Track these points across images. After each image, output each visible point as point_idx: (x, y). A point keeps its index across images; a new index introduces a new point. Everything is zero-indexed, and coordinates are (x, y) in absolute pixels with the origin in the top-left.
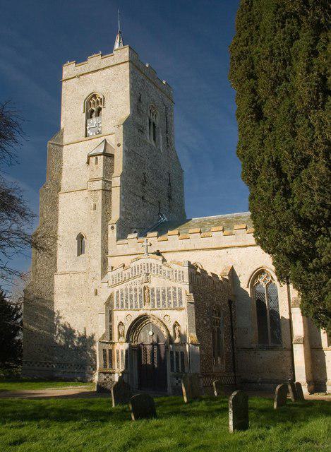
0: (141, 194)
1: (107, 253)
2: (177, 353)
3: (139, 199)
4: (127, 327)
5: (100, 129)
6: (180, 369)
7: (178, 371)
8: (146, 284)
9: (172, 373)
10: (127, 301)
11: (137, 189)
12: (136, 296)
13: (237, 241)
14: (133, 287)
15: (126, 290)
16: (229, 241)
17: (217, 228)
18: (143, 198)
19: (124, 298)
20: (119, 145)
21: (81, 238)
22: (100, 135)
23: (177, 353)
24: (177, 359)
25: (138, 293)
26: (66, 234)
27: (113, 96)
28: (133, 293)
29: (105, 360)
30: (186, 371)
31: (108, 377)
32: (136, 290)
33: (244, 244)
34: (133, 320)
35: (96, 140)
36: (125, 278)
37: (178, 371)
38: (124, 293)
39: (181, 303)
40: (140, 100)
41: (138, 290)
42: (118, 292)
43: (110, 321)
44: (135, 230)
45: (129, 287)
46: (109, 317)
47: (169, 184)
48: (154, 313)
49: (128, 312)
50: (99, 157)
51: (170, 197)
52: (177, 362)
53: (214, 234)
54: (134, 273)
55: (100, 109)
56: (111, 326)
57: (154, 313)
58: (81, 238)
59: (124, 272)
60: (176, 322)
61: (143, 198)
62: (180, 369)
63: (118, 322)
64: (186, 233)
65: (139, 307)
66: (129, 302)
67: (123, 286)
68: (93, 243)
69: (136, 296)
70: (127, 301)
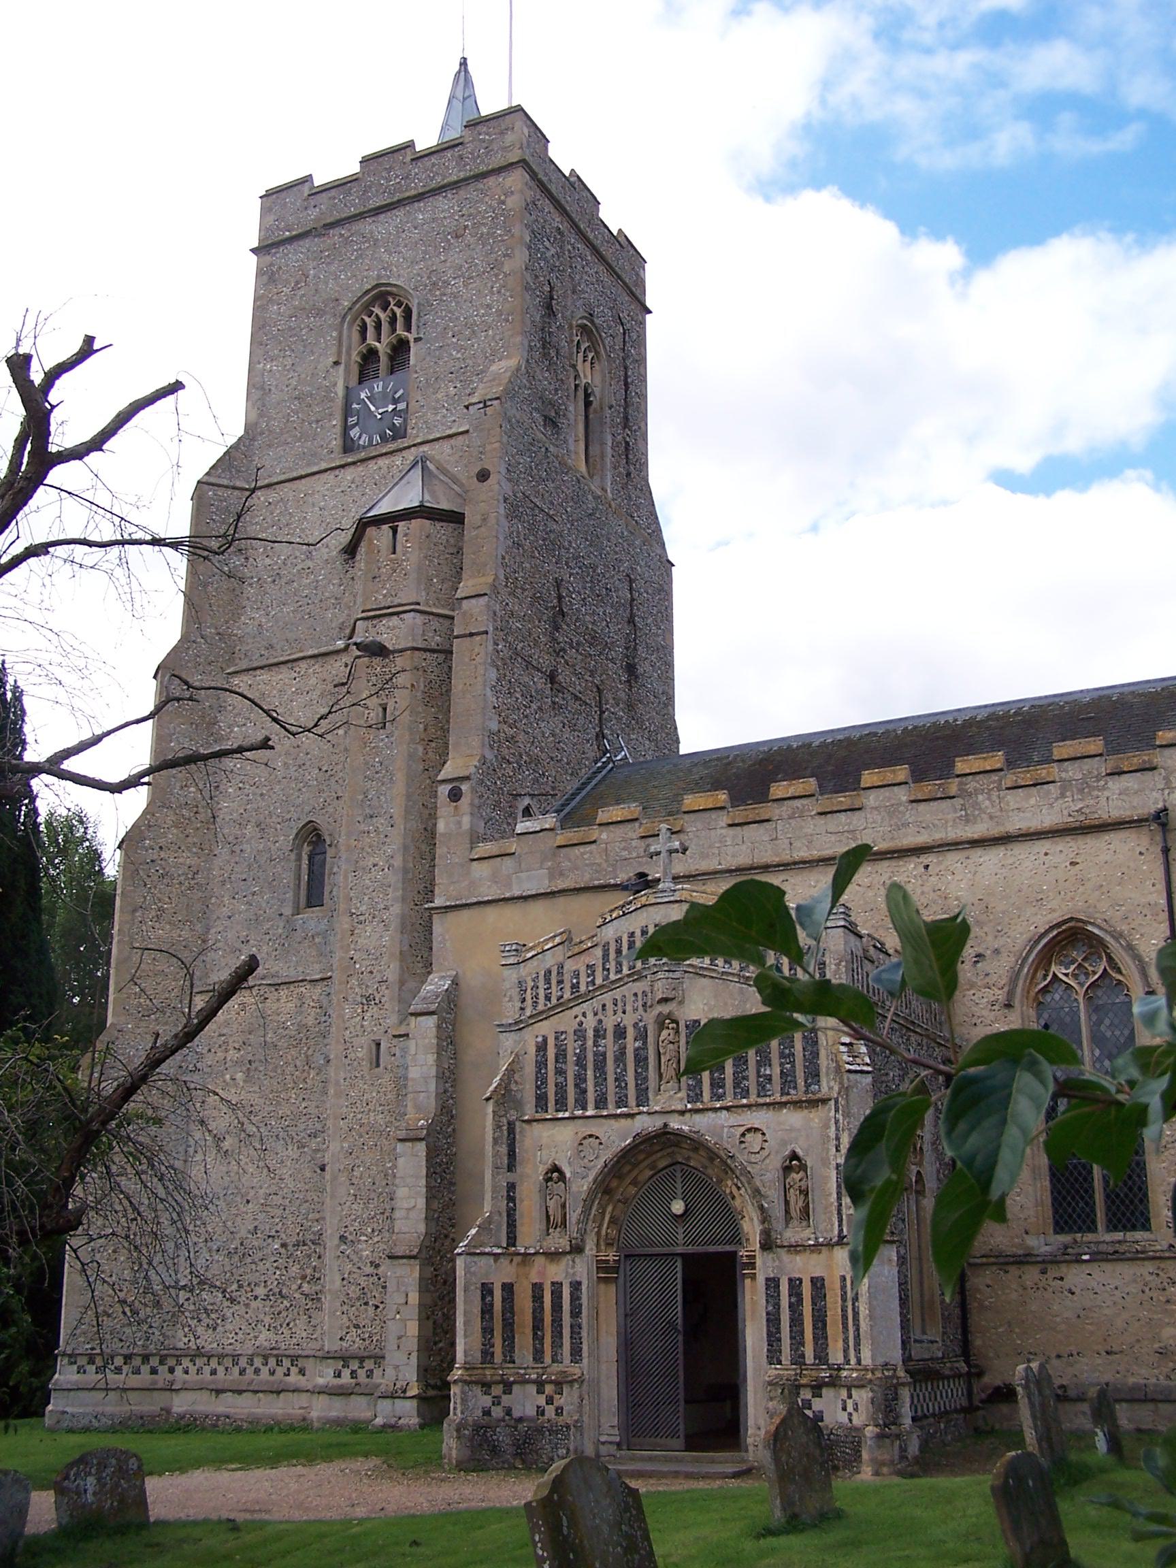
0: (546, 661)
1: (429, 893)
2: (795, 1284)
3: (540, 682)
4: (582, 1186)
5: (397, 421)
6: (809, 1351)
7: (798, 1359)
8: (665, 1009)
9: (773, 1371)
10: (580, 1079)
11: (536, 642)
12: (620, 1056)
13: (967, 820)
14: (609, 1023)
15: (580, 1034)
16: (938, 821)
17: (797, 787)
18: (552, 678)
19: (571, 1070)
20: (483, 476)
21: (313, 840)
22: (401, 443)
23: (795, 1285)
24: (795, 1307)
25: (631, 1044)
26: (250, 830)
27: (455, 296)
28: (609, 1045)
29: (487, 1331)
30: (836, 1357)
31: (497, 1401)
32: (620, 1033)
33: (996, 831)
34: (607, 1155)
35: (382, 462)
36: (575, 987)
37: (798, 1359)
38: (572, 1047)
39: (813, 1075)
40: (549, 307)
41: (631, 1033)
42: (542, 1047)
43: (511, 1167)
44: (527, 801)
45: (590, 1023)
46: (504, 1149)
47: (631, 621)
48: (702, 1123)
49: (586, 1128)
50: (402, 526)
51: (631, 669)
52: (796, 1321)
53: (871, 799)
54: (612, 965)
55: (400, 349)
56: (511, 1187)
57: (702, 1123)
58: (313, 840)
59: (570, 966)
60: (794, 1156)
61: (552, 678)
62: (809, 1351)
63: (542, 1169)
64: (1049, 760)
65: (632, 1101)
66: (590, 1085)
67: (566, 1022)
68: (369, 877)
69: (620, 1056)
70: (580, 1079)
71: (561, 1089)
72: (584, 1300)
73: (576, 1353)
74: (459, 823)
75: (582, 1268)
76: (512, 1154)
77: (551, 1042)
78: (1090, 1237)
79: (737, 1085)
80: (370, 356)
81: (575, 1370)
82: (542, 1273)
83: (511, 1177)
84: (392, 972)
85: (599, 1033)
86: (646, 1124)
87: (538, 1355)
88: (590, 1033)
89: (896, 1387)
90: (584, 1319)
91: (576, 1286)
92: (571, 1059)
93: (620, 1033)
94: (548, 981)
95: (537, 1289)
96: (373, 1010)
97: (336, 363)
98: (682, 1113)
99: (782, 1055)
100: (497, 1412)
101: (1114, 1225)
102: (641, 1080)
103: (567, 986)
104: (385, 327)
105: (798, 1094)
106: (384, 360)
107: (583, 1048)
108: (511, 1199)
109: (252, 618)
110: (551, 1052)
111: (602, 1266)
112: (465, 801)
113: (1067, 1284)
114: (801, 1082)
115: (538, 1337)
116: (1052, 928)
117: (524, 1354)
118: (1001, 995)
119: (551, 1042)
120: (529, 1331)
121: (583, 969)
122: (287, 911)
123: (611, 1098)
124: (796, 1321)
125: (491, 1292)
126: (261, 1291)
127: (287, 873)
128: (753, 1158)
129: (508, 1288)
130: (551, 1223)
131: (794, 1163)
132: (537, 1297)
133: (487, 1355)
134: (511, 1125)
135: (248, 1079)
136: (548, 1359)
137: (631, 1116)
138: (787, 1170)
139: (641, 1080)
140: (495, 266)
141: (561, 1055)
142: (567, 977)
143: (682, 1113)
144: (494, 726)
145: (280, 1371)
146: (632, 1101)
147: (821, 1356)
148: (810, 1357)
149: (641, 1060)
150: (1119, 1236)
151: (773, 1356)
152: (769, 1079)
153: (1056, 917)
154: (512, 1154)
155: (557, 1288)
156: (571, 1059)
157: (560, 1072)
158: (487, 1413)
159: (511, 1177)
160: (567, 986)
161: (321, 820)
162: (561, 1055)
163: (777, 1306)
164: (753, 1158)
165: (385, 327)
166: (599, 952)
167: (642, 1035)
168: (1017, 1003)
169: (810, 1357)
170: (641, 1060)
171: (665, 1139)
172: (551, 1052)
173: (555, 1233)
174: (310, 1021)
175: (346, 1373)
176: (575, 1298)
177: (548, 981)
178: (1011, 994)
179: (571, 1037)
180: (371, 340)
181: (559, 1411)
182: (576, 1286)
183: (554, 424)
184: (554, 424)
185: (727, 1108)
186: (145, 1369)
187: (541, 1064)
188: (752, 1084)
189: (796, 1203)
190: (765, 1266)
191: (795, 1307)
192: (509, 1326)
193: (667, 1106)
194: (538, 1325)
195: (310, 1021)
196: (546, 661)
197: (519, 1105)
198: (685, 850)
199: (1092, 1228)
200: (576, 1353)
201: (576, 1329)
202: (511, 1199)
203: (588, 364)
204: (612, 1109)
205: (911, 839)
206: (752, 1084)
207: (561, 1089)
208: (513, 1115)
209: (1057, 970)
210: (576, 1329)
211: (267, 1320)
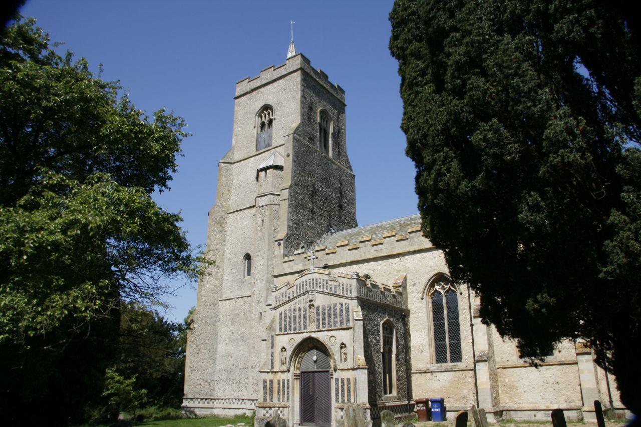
0: (310, 206)
6: (346, 398)
7: (343, 401)
10: (290, 323)
12: (300, 317)
18: (312, 211)
19: (288, 320)
24: (284, 386)
27: (284, 106)
30: (352, 401)
31: (267, 412)
32: (300, 310)
33: (420, 248)
34: (296, 344)
36: (289, 297)
37: (343, 401)
38: (288, 315)
39: (348, 320)
41: (302, 310)
42: (281, 314)
43: (272, 348)
44: (302, 245)
45: (293, 307)
51: (340, 206)
52: (343, 390)
55: (271, 121)
56: (272, 353)
58: (248, 257)
61: (312, 211)
62: (346, 398)
63: (281, 348)
65: (302, 328)
66: (292, 324)
67: (286, 307)
71: (285, 325)
72: (290, 385)
73: (288, 399)
74: (280, 252)
75: (289, 376)
76: (273, 344)
77: (283, 313)
78: (445, 364)
79: (329, 324)
80: (263, 125)
81: (288, 404)
82: (280, 377)
83: (272, 350)
84: (264, 293)
85: (295, 310)
86: (305, 335)
87: (279, 399)
88: (293, 310)
89: (366, 409)
90: (290, 390)
91: (288, 381)
92: (288, 317)
93: (300, 310)
94: (283, 295)
95: (279, 381)
96: (260, 304)
97: (255, 127)
98: (315, 332)
99: (340, 315)
100: (267, 415)
101: (452, 361)
102: (305, 322)
103: (287, 297)
104: (267, 116)
105: (344, 326)
106: (267, 125)
107: (291, 315)
108: (272, 356)
109: (233, 198)
110: (283, 315)
111: (295, 375)
112: (282, 246)
113: (438, 378)
114: (345, 323)
115: (279, 395)
116: (434, 276)
117: (275, 400)
118: (420, 295)
119: (283, 313)
120: (277, 393)
121: (291, 292)
122: (242, 277)
123: (298, 328)
124: (343, 390)
125: (266, 382)
126: (235, 381)
127: (242, 265)
128: (333, 344)
129: (271, 381)
130: (283, 363)
131: (343, 346)
132: (279, 384)
133: (265, 399)
134: (272, 337)
135: (232, 324)
136: (281, 401)
137: (302, 333)
138: (341, 348)
139: (305, 322)
140: (294, 97)
141: (285, 316)
142: (287, 295)
143: (315, 332)
144: (291, 224)
145: (239, 403)
146: (302, 328)
147: (349, 400)
148: (346, 401)
149: (305, 317)
150: (453, 364)
151: (337, 400)
152: (337, 322)
153: (435, 272)
154: (273, 344)
155: (348, 380)
156: (288, 317)
157: (285, 321)
158: (264, 415)
159: (272, 350)
160: (287, 297)
161: (251, 253)
162: (285, 316)
163: (338, 386)
164: (333, 344)
165: (267, 116)
166: (295, 287)
167: (305, 310)
168: (425, 297)
169: (346, 401)
170: (305, 317)
171: (310, 339)
172: (283, 315)
173: (284, 366)
174: (247, 307)
175: (253, 404)
176: (288, 384)
177: (283, 295)
178: (423, 295)
179: (288, 311)
180: (263, 120)
181: (283, 415)
182: (288, 381)
183: (313, 140)
184: (313, 140)
185: (326, 331)
186: (201, 402)
187: (281, 319)
188: (332, 323)
189: (343, 357)
190: (335, 375)
191: (284, 386)
192: (271, 391)
193: (312, 331)
194: (279, 392)
195: (247, 307)
196: (310, 206)
197: (274, 330)
198: (317, 258)
199: (446, 362)
200: (288, 399)
201: (288, 392)
202: (272, 356)
203: (325, 122)
204: (298, 331)
205: (396, 252)
206: (332, 323)
207: (285, 325)
208: (273, 333)
209: (437, 287)
210: (288, 394)
211: (236, 389)
